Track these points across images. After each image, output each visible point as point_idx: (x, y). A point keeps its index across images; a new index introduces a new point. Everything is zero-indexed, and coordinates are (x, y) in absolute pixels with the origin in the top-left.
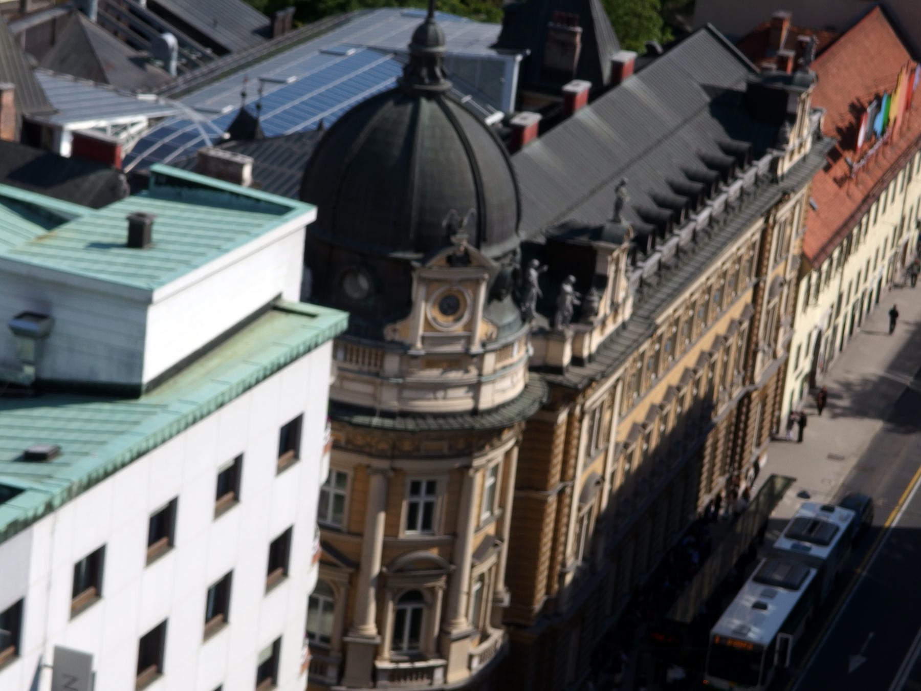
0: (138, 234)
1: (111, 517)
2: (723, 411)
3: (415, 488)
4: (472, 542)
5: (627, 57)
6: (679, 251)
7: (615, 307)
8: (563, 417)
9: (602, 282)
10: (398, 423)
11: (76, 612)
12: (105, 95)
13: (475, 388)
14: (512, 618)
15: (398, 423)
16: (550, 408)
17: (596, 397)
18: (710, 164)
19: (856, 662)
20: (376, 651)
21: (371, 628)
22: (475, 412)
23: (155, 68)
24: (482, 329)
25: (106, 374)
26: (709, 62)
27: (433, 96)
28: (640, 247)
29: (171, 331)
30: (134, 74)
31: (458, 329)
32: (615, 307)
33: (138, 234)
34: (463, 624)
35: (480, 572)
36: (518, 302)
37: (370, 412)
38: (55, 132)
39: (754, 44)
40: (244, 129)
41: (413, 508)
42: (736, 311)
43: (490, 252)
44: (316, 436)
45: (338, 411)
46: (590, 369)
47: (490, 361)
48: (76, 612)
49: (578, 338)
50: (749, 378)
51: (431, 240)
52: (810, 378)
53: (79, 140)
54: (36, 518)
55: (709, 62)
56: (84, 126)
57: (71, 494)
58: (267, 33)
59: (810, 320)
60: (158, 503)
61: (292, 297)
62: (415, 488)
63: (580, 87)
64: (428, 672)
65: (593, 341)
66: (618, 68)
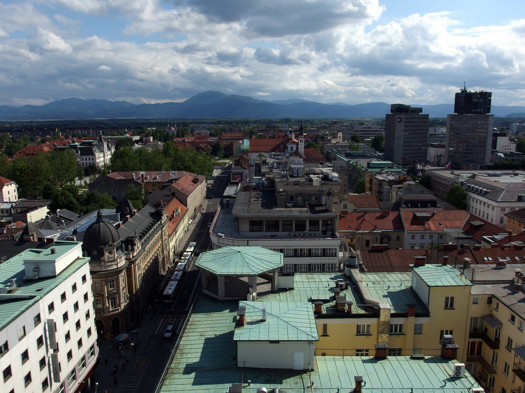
0: (53, 252)
1: (54, 296)
2: (160, 260)
3: (110, 282)
4: (121, 288)
5: (135, 210)
6: (147, 237)
7: (138, 248)
8: (133, 266)
9: (135, 245)
10: (105, 272)
11: (50, 313)
12: (52, 231)
13: (117, 264)
14: (130, 299)
15: (105, 272)
16: (130, 265)
17: (137, 262)
18: (151, 224)
19: (186, 292)
20: (109, 308)
21: (107, 305)
22: (118, 268)
23: (61, 226)
24: (116, 255)
25: (50, 275)
26: (149, 209)
27: (102, 222)
28: (141, 238)
29: (60, 265)
30: (58, 227)
31: (112, 256)
32: (138, 248)
33: (53, 252)
34: (122, 301)
35: (124, 292)
36: (122, 250)
37: (101, 272)
38: (44, 239)
39: (157, 205)
40: (75, 232)
41: (111, 285)
42: (159, 245)
43: (115, 244)
44: (89, 277)
45: (92, 273)
46: (135, 258)
47: (118, 260)
48: (50, 313)
49: (133, 253)
50: (163, 254)
51: (105, 243)
52: (174, 252)
53: (47, 239)
54: (39, 300)
55: (149, 209)
56: (49, 237)
57: (45, 295)
58: (79, 217)
59: (172, 244)
60: (62, 293)
61: (81, 256)
62: (110, 282)
63: (128, 216)
64: (118, 309)
65: (135, 253)
66: (134, 212)
